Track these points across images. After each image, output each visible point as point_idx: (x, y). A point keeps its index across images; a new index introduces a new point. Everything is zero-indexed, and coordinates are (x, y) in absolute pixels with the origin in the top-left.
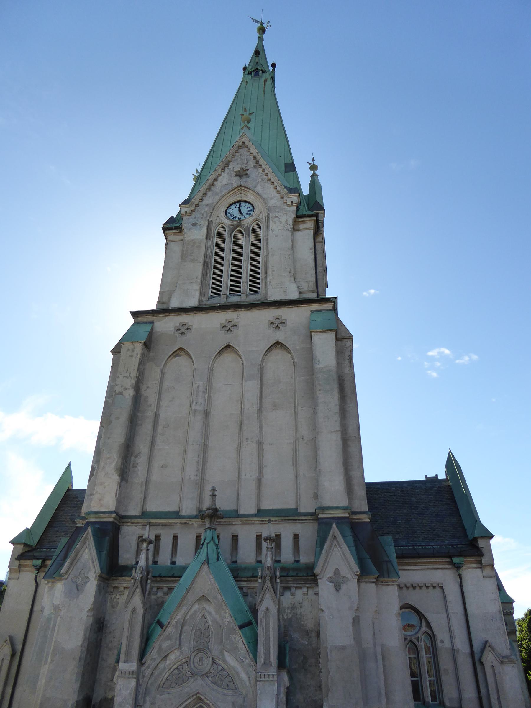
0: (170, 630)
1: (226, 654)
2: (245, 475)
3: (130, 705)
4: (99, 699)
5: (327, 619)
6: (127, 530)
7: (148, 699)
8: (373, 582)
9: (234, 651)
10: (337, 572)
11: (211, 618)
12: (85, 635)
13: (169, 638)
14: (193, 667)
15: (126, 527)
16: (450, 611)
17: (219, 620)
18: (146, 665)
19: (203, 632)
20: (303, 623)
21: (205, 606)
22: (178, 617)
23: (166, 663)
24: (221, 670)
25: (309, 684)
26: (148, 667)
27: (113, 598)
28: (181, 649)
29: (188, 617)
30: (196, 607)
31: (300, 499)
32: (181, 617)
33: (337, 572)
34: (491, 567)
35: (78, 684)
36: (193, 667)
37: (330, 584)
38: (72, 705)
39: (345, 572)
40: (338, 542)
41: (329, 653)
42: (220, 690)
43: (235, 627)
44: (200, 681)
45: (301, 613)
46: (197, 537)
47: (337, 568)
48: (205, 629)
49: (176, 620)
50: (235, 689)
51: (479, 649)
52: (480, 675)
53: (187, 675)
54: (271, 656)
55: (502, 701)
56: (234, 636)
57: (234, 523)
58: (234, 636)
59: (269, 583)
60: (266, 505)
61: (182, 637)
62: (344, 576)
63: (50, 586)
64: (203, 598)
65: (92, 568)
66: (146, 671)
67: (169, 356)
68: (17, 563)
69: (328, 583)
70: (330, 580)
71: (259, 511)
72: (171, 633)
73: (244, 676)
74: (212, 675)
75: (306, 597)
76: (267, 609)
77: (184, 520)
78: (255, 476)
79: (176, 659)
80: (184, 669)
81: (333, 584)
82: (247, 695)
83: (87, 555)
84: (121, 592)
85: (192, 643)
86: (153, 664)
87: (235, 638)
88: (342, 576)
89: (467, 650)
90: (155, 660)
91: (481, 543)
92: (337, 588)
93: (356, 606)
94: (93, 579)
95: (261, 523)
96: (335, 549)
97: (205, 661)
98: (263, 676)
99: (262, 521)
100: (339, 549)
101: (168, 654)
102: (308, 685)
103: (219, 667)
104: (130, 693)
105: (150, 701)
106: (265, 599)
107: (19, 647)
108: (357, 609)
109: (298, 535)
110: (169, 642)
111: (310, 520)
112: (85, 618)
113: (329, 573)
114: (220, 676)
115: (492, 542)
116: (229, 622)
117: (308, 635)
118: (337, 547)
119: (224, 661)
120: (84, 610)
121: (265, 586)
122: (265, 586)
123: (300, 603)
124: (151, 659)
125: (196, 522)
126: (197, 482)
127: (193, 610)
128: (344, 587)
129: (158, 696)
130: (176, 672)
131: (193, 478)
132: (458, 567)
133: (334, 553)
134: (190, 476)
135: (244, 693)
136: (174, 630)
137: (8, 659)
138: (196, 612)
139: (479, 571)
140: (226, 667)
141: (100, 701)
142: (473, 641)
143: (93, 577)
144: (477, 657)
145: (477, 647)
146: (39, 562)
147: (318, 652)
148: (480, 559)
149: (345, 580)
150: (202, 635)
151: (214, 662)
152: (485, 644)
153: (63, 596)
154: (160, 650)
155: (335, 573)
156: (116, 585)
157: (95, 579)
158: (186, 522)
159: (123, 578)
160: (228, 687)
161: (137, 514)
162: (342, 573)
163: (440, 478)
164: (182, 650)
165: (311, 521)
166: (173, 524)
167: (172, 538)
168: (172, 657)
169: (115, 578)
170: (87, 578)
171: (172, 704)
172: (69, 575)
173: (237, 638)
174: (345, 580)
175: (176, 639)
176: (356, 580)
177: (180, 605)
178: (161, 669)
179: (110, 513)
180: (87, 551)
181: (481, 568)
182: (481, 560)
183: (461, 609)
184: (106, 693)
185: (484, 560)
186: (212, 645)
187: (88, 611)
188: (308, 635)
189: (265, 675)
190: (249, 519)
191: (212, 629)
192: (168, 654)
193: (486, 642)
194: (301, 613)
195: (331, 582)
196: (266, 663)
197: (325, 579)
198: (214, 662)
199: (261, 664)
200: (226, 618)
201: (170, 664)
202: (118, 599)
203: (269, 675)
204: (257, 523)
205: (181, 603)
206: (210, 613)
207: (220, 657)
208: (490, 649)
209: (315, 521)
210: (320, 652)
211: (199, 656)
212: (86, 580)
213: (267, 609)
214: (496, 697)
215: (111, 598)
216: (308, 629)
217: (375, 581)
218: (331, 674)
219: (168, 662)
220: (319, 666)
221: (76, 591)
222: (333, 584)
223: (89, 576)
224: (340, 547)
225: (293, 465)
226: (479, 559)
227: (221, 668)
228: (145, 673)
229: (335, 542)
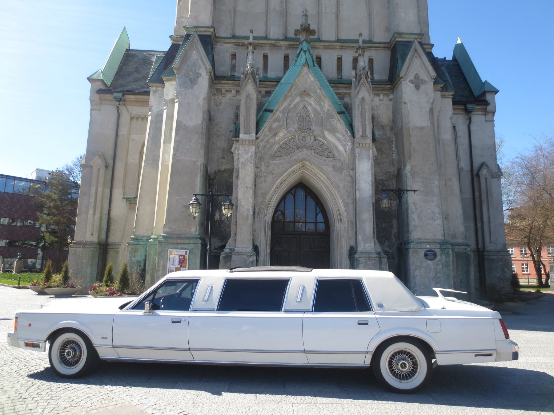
0: (278, 114)
1: (326, 133)
2: (325, 9)
3: (252, 164)
4: (213, 172)
5: (409, 108)
6: (220, 48)
7: (262, 163)
8: (439, 91)
9: (333, 131)
10: (417, 76)
11: (312, 108)
12: (203, 116)
13: (277, 120)
14: (298, 142)
15: (219, 46)
16: (459, 143)
17: (318, 108)
18: (260, 139)
19: (305, 118)
20: (379, 120)
21: (306, 99)
22: (284, 106)
23: (275, 139)
24: (322, 145)
25: (384, 161)
26: (262, 141)
27: (216, 99)
28: (287, 129)
29: (292, 106)
30: (298, 99)
31: (374, 31)
32: (286, 105)
33: (417, 76)
34: (492, 113)
35: (275, 77)
36: (298, 142)
37: (412, 84)
38: (200, 165)
39: (424, 76)
40: (418, 54)
41: (411, 132)
42: (323, 158)
43: (333, 113)
44: (305, 151)
45: (378, 113)
46: (285, 57)
47: (417, 74)
48: (307, 116)
49: (282, 108)
50: (334, 157)
51: (477, 168)
52: (476, 185)
53: (293, 147)
54: (367, 131)
55: (489, 199)
56: (333, 120)
57: (318, 47)
58: (333, 120)
59: (365, 79)
60: (344, 36)
61: (288, 121)
62: (423, 79)
63: (154, 90)
64: (305, 93)
65: (202, 66)
66: (260, 144)
67: (96, 74)
68: (97, 96)
69: (410, 84)
70: (411, 81)
71: (338, 39)
72: (279, 117)
73: (341, 148)
74: (315, 148)
75: (382, 102)
76: (363, 98)
77: (273, 42)
78: (334, 11)
79: (284, 136)
80: (291, 144)
81: (414, 84)
82: (344, 161)
83: (195, 56)
84: (224, 94)
85: (297, 126)
86: (266, 139)
87: (334, 121)
88: (421, 80)
89: (469, 168)
90: (267, 136)
91: (488, 97)
92: (417, 87)
93: (431, 101)
94: (205, 74)
95: (341, 48)
96: (416, 59)
97: (308, 139)
98: (361, 145)
99: (342, 46)
100: (419, 59)
101: (277, 132)
102: (384, 162)
103: (320, 143)
104: (251, 156)
105: (265, 165)
106: (361, 91)
107: (110, 162)
108: (432, 104)
109: (373, 59)
110: (278, 123)
111: (383, 47)
112: (201, 103)
113: (411, 77)
114: (321, 149)
115: (497, 96)
116: (328, 110)
117: (383, 128)
118: (417, 59)
119: (324, 138)
120: (200, 97)
121: (362, 81)
122: (360, 83)
123: (377, 106)
124: (264, 135)
125: (283, 44)
126: (282, 12)
127: (296, 102)
128: (422, 87)
129: (271, 162)
130: (285, 145)
131: (278, 8)
132: (468, 112)
133: (414, 63)
134: (274, 7)
135: (342, 160)
136: (281, 115)
137: (103, 169)
138: (298, 103)
139: (482, 117)
140: (325, 142)
141: (215, 172)
142: (473, 163)
143: (204, 73)
144: (475, 173)
145: (476, 165)
146: (120, 95)
147: (391, 140)
148: (486, 108)
149: (423, 82)
150: (305, 121)
151: (315, 139)
152: (483, 165)
153: (178, 87)
154: (271, 129)
155: (415, 77)
156: (219, 87)
157: (206, 74)
158: (274, 44)
159: (226, 82)
160: (328, 156)
161: (228, 36)
162: (421, 77)
163: (447, 59)
164: (289, 130)
165: (384, 49)
166: (263, 45)
167: (262, 56)
168: (281, 134)
169: (218, 81)
170: (198, 73)
171: (283, 167)
172: (181, 70)
173: (335, 121)
174: (423, 82)
175: (284, 122)
176: (432, 83)
177: (286, 97)
178: (271, 143)
179: (209, 27)
180: (194, 52)
181: (485, 115)
182: (486, 109)
183: (466, 141)
184: (218, 167)
185: (489, 108)
186: (313, 127)
187: (203, 99)
188: (383, 128)
189: (363, 144)
190: (331, 44)
191: (313, 116)
192: (277, 132)
193: (484, 163)
194: (378, 113)
195: (412, 83)
196: (363, 136)
197: (407, 81)
198: (315, 139)
199: (359, 136)
200: (325, 107)
201: (279, 140)
202: (221, 99)
203: (366, 144)
204: (338, 47)
205: (287, 95)
206: (310, 104)
207: (321, 135)
208: (485, 167)
209: (387, 49)
210: (392, 140)
211: (303, 134)
212: (198, 75)
213: (363, 98)
214: (486, 196)
215: (215, 99)
216: (383, 124)
217: (441, 89)
218: (413, 145)
219: (277, 138)
220: (392, 150)
221: (190, 83)
222: (414, 84)
223: (200, 71)
224: (420, 57)
225: (366, 5)
226: (484, 107)
227: (321, 143)
228: (260, 145)
229: (416, 54)
